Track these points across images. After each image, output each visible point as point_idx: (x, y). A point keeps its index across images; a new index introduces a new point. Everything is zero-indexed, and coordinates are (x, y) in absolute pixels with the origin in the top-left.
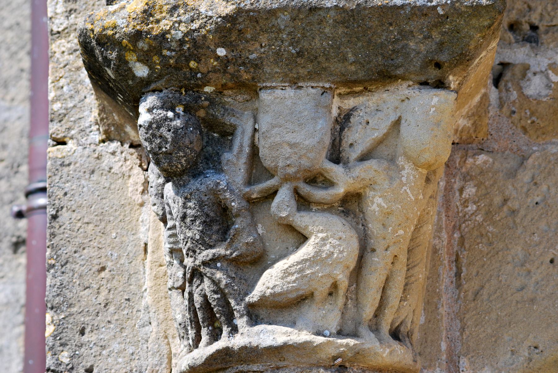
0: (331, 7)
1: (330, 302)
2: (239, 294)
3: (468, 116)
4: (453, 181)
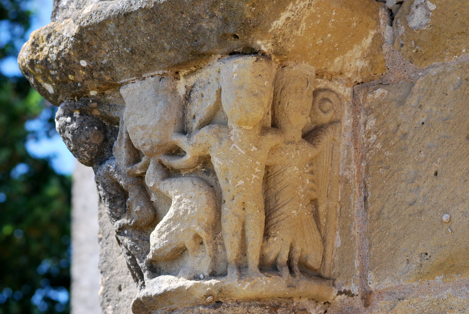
0: (137, 10)
1: (202, 250)
2: (142, 253)
3: (364, 57)
4: (358, 116)
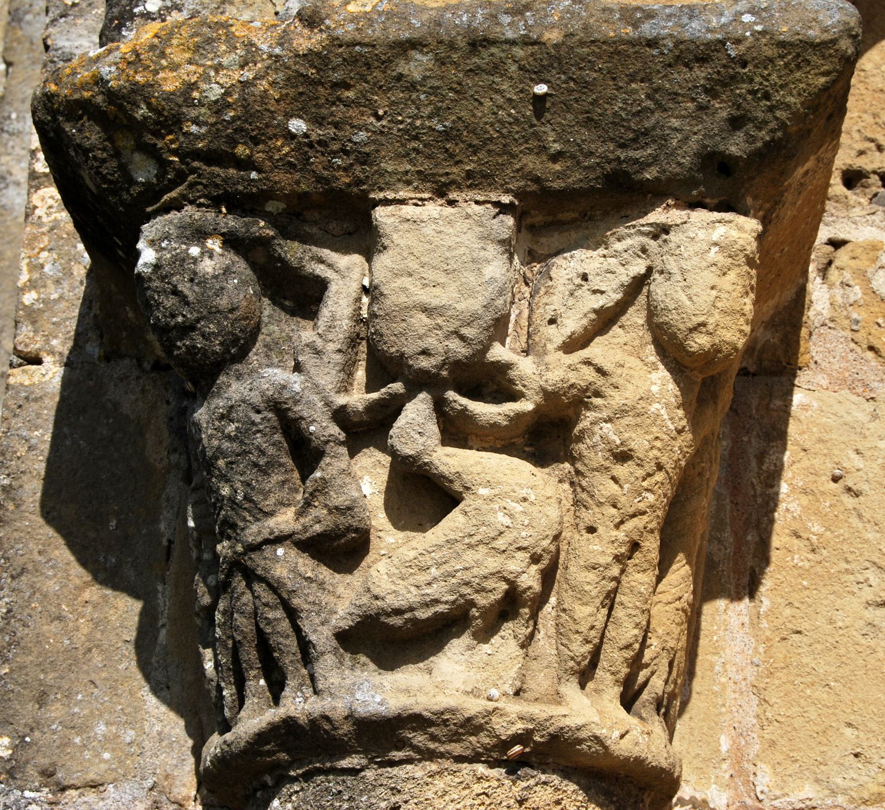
4: (745, 439)
